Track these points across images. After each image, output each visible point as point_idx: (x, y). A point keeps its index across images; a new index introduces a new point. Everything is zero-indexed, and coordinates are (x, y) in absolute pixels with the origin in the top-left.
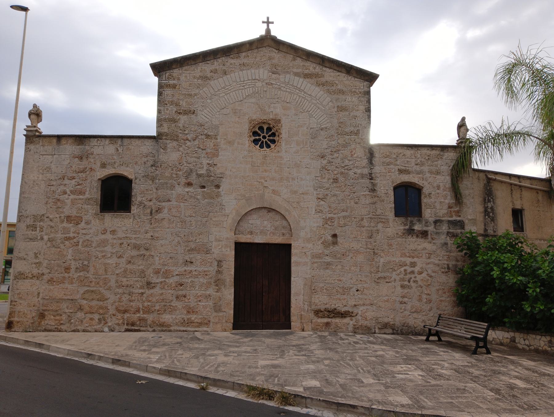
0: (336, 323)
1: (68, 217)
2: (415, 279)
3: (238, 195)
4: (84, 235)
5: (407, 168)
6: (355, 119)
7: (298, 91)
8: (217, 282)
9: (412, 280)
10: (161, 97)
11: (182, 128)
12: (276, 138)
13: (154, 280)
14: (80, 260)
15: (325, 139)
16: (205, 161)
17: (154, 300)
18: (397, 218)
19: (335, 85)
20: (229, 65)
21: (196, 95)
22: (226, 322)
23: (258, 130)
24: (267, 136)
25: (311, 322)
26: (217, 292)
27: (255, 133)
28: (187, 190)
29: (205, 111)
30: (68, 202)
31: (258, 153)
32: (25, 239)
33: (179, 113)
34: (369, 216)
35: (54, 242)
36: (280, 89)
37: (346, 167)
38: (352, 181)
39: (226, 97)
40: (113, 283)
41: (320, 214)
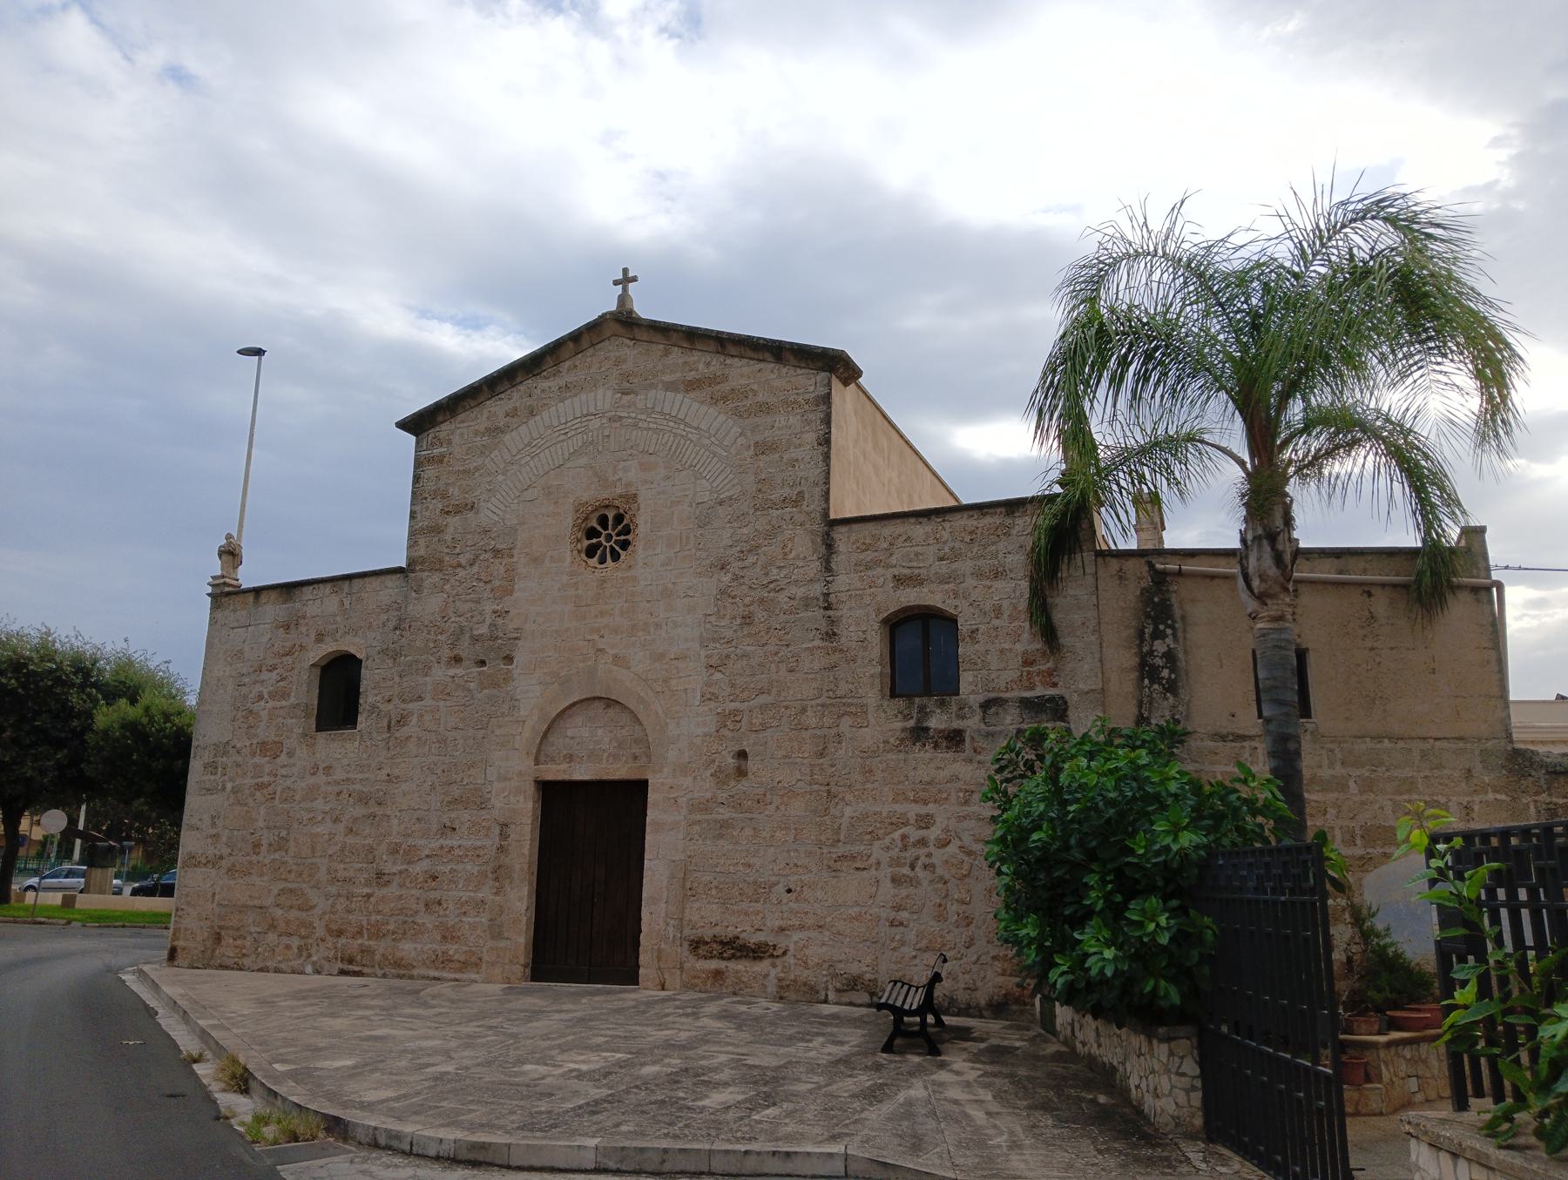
3: (545, 673)
22: (511, 961)
25: (681, 968)
26: (496, 894)
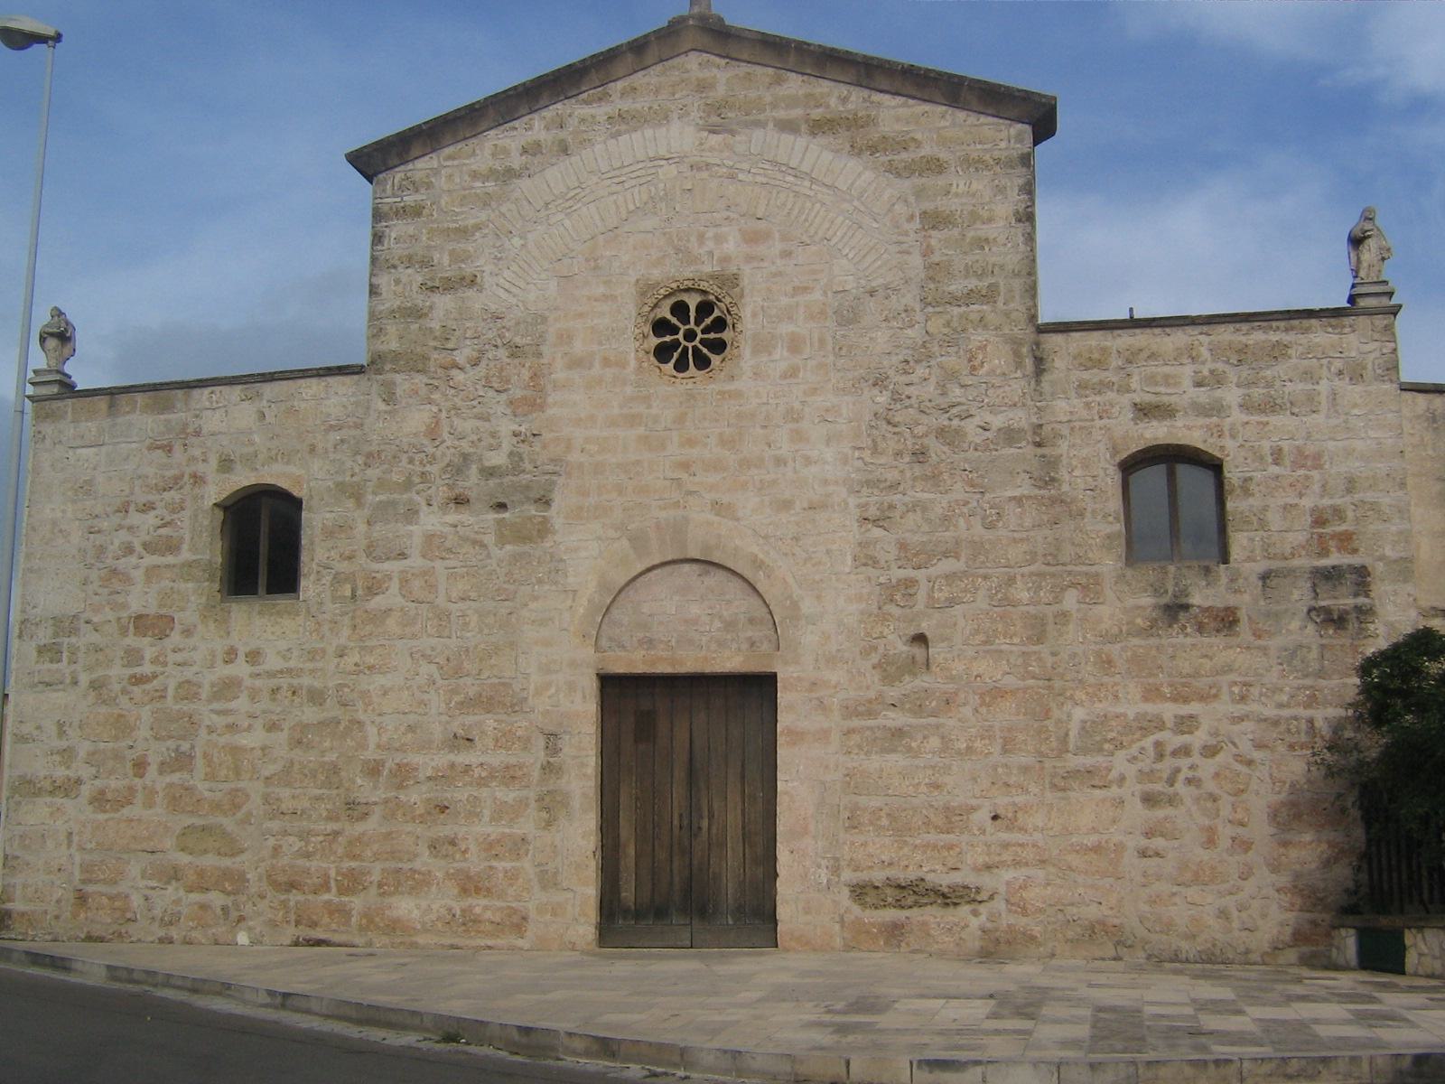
0: (925, 924)
1: (139, 617)
2: (1190, 774)
4: (180, 668)
5: (1165, 399)
6: (982, 248)
7: (790, 179)
9: (1181, 777)
10: (379, 248)
11: (438, 334)
12: (726, 335)
13: (365, 790)
14: (170, 737)
15: (884, 324)
16: (506, 427)
18: (1129, 573)
19: (913, 145)
20: (576, 124)
21: (478, 227)
23: (669, 316)
24: (698, 330)
27: (661, 327)
28: (452, 517)
29: (506, 273)
30: (138, 575)
31: (668, 386)
32: (35, 685)
33: (433, 289)
34: (1033, 568)
35: (104, 691)
36: (732, 177)
37: (954, 411)
38: (972, 454)
39: (567, 223)
40: (255, 804)
41: (870, 571)
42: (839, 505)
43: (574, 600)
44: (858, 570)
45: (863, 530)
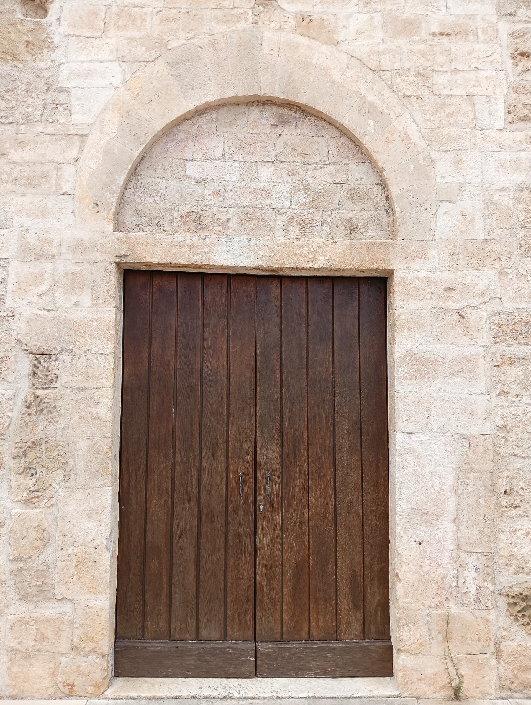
3: (131, 39)
8: (31, 454)
17: (508, 382)
22: (75, 648)
25: (498, 654)
26: (28, 502)
42: (485, 31)
43: (81, 150)
44: (514, 126)
45: (519, 69)
